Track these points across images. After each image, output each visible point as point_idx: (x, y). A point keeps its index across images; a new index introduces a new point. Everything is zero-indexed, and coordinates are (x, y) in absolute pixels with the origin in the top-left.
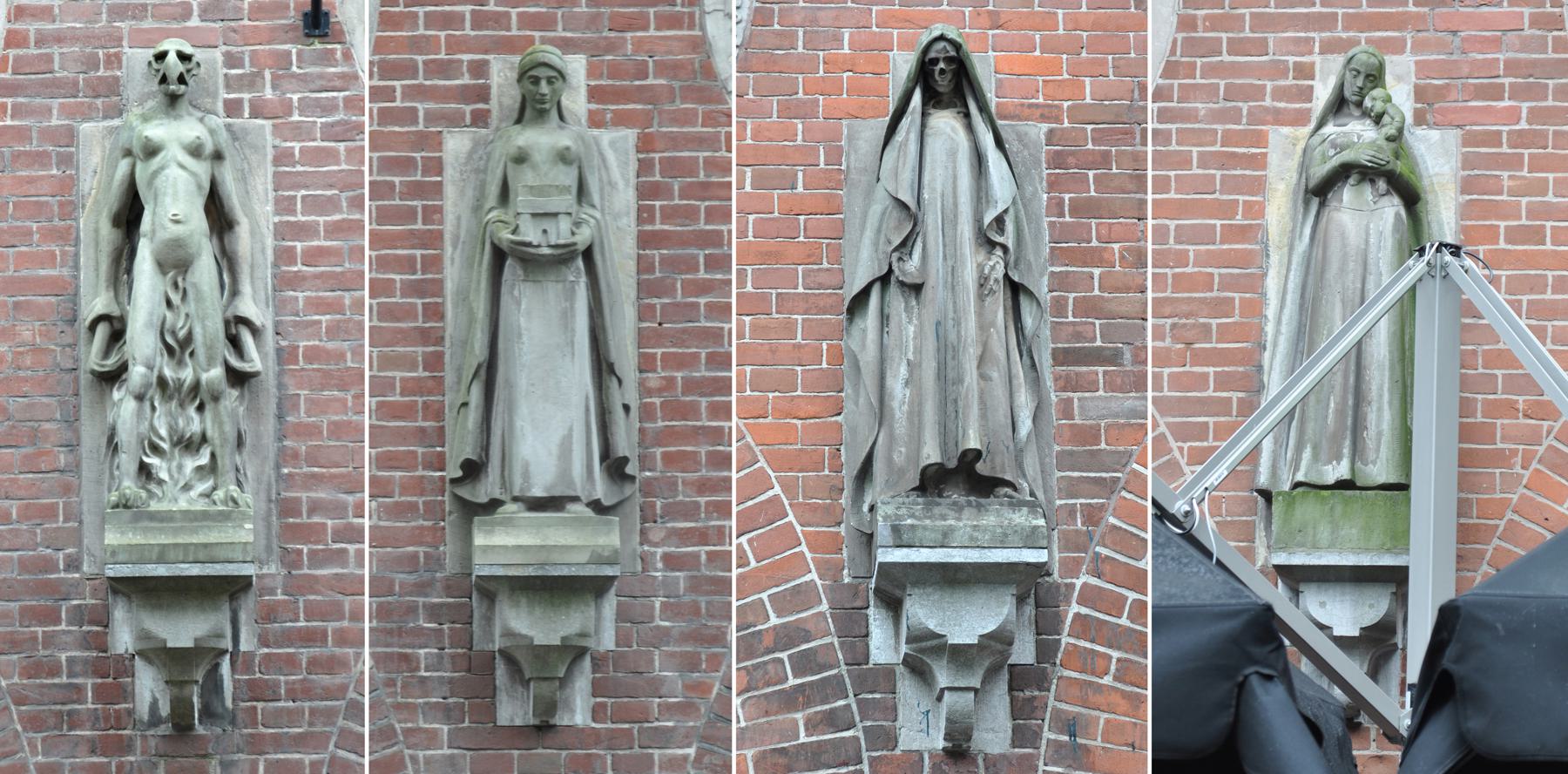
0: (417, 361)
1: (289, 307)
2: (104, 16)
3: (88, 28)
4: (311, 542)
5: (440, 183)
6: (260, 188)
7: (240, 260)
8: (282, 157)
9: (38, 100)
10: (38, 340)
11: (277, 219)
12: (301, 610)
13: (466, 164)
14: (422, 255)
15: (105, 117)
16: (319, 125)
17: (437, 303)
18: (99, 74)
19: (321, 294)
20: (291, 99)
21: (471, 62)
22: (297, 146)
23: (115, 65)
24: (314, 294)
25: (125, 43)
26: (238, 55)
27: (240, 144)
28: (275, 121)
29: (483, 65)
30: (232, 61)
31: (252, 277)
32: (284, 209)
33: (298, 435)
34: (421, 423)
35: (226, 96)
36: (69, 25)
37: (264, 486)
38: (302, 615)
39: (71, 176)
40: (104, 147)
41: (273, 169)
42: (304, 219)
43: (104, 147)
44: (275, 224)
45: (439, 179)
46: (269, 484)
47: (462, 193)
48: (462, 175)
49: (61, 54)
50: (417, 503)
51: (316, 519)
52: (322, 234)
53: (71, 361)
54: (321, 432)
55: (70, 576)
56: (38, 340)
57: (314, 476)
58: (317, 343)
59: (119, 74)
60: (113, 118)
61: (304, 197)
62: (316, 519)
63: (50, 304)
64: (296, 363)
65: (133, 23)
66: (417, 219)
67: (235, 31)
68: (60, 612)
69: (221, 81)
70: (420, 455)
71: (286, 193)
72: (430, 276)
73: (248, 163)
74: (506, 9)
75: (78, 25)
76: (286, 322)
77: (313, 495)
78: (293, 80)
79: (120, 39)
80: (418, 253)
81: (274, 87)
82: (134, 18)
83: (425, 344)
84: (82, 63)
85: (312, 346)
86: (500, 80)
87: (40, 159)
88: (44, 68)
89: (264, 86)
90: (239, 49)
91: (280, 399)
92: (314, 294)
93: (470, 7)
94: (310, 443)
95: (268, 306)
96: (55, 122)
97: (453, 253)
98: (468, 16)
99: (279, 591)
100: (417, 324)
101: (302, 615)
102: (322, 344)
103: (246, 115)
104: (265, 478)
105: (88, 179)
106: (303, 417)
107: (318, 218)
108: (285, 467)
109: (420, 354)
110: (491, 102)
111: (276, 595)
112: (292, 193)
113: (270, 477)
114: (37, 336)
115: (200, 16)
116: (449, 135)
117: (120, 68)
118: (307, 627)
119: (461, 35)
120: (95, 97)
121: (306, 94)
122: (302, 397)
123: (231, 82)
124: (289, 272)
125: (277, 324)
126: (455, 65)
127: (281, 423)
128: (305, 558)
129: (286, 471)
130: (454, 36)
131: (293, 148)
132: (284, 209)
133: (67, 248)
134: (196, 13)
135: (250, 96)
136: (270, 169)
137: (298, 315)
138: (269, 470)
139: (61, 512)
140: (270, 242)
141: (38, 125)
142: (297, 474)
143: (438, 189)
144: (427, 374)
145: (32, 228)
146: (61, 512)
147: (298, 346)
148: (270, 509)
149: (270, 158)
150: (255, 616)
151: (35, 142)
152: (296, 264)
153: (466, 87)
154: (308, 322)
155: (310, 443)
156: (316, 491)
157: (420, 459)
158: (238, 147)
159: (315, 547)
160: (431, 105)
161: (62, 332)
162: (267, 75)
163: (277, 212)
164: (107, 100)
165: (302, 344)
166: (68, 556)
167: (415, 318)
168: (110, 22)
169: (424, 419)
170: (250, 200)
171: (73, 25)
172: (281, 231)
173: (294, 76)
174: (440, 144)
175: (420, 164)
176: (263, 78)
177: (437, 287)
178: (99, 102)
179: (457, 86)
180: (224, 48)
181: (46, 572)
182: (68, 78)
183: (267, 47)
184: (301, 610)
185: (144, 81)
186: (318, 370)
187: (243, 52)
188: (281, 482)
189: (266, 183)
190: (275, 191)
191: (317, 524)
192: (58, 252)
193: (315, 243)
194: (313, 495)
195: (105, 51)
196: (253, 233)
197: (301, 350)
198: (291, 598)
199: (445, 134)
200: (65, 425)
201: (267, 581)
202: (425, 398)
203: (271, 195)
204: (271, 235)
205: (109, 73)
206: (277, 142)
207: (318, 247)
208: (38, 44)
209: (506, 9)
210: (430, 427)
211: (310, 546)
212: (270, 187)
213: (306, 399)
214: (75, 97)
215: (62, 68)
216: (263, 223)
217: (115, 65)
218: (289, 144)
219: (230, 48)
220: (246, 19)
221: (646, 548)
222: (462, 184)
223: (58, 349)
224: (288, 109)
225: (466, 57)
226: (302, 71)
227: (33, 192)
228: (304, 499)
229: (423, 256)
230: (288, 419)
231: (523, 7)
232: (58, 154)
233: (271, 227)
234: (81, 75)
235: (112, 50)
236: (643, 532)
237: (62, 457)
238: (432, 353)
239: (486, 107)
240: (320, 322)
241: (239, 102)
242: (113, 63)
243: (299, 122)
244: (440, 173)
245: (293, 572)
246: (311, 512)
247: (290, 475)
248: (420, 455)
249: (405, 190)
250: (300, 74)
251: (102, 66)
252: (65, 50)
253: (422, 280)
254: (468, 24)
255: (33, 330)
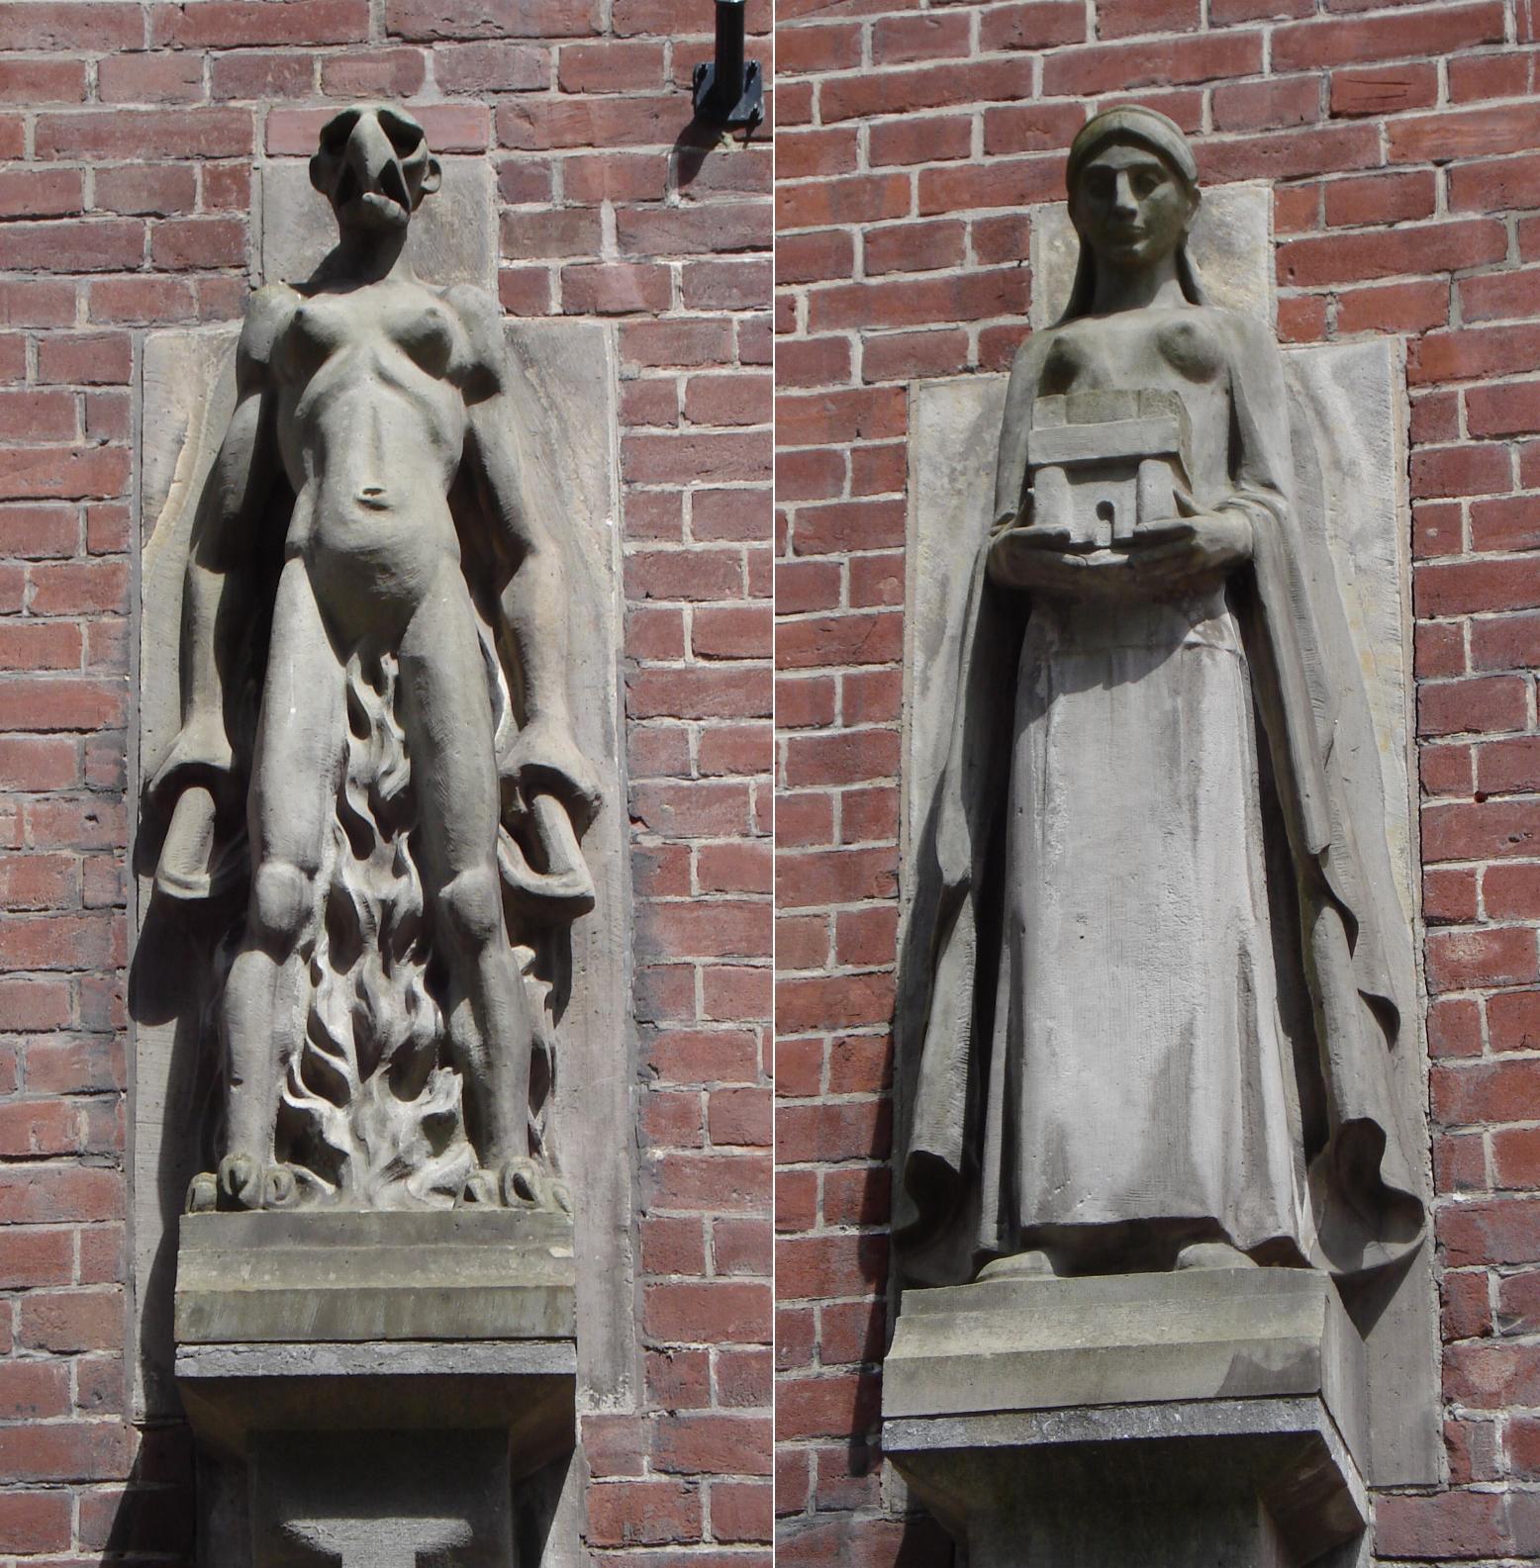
0: (824, 940)
1: (663, 755)
2: (207, 86)
3: (168, 113)
4: (727, 1336)
5: (901, 506)
6: (588, 474)
7: (538, 637)
8: (640, 406)
9: (42, 278)
10: (30, 837)
11: (631, 548)
12: (706, 1512)
13: (964, 456)
14: (847, 679)
15: (207, 318)
16: (736, 327)
17: (882, 790)
18: (191, 217)
19: (744, 723)
20: (667, 268)
21: (981, 226)
22: (681, 377)
23: (233, 197)
24: (726, 724)
25: (257, 146)
26: (534, 171)
27: (538, 375)
28: (625, 320)
29: (1014, 228)
30: (517, 184)
31: (569, 686)
32: (650, 525)
33: (689, 1066)
34: (825, 1098)
35: (505, 264)
36: (120, 106)
37: (602, 1191)
38: (707, 1525)
39: (121, 455)
40: (202, 382)
41: (623, 431)
42: (699, 547)
43: (202, 382)
44: (626, 558)
45: (898, 496)
46: (616, 1188)
47: (954, 522)
48: (953, 480)
49: (98, 172)
50: (808, 1315)
51: (739, 1277)
52: (746, 581)
53: (111, 886)
54: (751, 1059)
55: (95, 1420)
56: (30, 837)
57: (731, 1165)
58: (736, 840)
59: (241, 215)
60: (225, 320)
61: (697, 496)
62: (739, 1277)
63: (60, 752)
64: (685, 889)
65: (277, 100)
66: (838, 594)
67: (526, 115)
68: (68, 1514)
69: (493, 226)
70: (820, 1181)
71: (655, 488)
72: (864, 727)
73: (560, 418)
74: (1072, 99)
75: (143, 107)
76: (658, 790)
77: (731, 1214)
78: (673, 226)
79: (246, 137)
80: (838, 673)
81: (624, 241)
82: (279, 89)
83: (848, 892)
84: (152, 193)
85: (720, 848)
86: (1054, 257)
87: (46, 412)
88: (56, 204)
89: (599, 241)
90: (539, 156)
91: (640, 976)
92: (726, 724)
93: (982, 106)
94: (720, 1085)
95: (609, 754)
96: (82, 327)
97: (926, 667)
98: (977, 126)
99: (646, 1461)
100: (827, 848)
101: (707, 1525)
102: (749, 842)
103: (555, 307)
104: (605, 1172)
105: (163, 459)
106: (702, 1022)
107: (736, 545)
108: (656, 1143)
109: (833, 920)
110: (1031, 309)
111: (638, 1472)
112: (669, 487)
113: (617, 1167)
114: (28, 828)
115: (440, 82)
116: (923, 394)
117: (244, 202)
118: (721, 1555)
119: (960, 169)
120: (183, 270)
121: (703, 258)
122: (699, 972)
123: (519, 232)
124: (663, 672)
125: (632, 797)
126: (939, 236)
127: (643, 1036)
128: (714, 1377)
129: (659, 1153)
130: (941, 171)
131: (673, 381)
132: (650, 525)
133: (106, 619)
134: (430, 77)
135: (563, 263)
136: (615, 432)
137: (687, 776)
138: (616, 1155)
139: (77, 1257)
140: (614, 602)
141: (41, 334)
142: (690, 1162)
143: (894, 520)
144: (850, 969)
145: (21, 573)
146: (77, 1257)
147: (688, 849)
148: (618, 1252)
149: (613, 406)
150: (582, 1529)
151: (31, 374)
152: (681, 654)
153: (971, 281)
154: (709, 789)
155: (720, 1085)
156: (738, 1204)
157: (820, 1196)
158: (535, 381)
159: (738, 1348)
160: (883, 332)
161: (91, 818)
162: (607, 214)
163: (631, 533)
164: (209, 275)
165: (695, 843)
166: (92, 1369)
167: (825, 833)
168: (219, 100)
169: (837, 1088)
170: (563, 503)
171: (131, 106)
172: (641, 576)
173: (673, 213)
174: (904, 415)
175: (849, 466)
176: (597, 221)
177: (885, 752)
178: (191, 281)
179: (948, 282)
180: (501, 155)
181: (34, 1411)
182: (116, 226)
183: (607, 151)
184: (706, 1512)
185: (301, 231)
186: (739, 905)
187: (545, 164)
188: (645, 1181)
189: (604, 463)
190: (627, 482)
191: (742, 1287)
192: (84, 630)
193: (728, 604)
194: (731, 1214)
195: (209, 164)
196: (568, 578)
197: (694, 859)
198: (679, 1480)
199: (913, 391)
200: (89, 1039)
201: (611, 1434)
202: (842, 1033)
203: (617, 490)
204: (618, 584)
205: (216, 215)
206: (633, 369)
207: (738, 611)
208: (43, 150)
209: (1072, 99)
210: (851, 1105)
211: (725, 1345)
212: (614, 474)
213: (707, 976)
214: (132, 270)
215: (103, 204)
216: (595, 556)
217: (233, 197)
218: (662, 373)
219: (516, 155)
220: (554, 88)
221: (1460, 1410)
222: (955, 502)
223: (79, 857)
224: (658, 291)
225: (970, 215)
226: (692, 205)
227: (24, 489)
228: (708, 1226)
229: (847, 679)
230: (663, 1025)
231: (1113, 89)
232: (88, 400)
233: (618, 567)
234: (150, 221)
235: (225, 163)
236: (1450, 1366)
237: (83, 1118)
238: (864, 915)
239: (1019, 320)
240: (743, 791)
241: (538, 277)
242: (228, 190)
243: (684, 321)
244: (900, 484)
245: (682, 1412)
246: (727, 1257)
247: (670, 1164)
248: (820, 1181)
249: (809, 530)
250: (688, 212)
251: (199, 199)
252: (109, 163)
253: (845, 737)
254: (977, 143)
255: (19, 814)
